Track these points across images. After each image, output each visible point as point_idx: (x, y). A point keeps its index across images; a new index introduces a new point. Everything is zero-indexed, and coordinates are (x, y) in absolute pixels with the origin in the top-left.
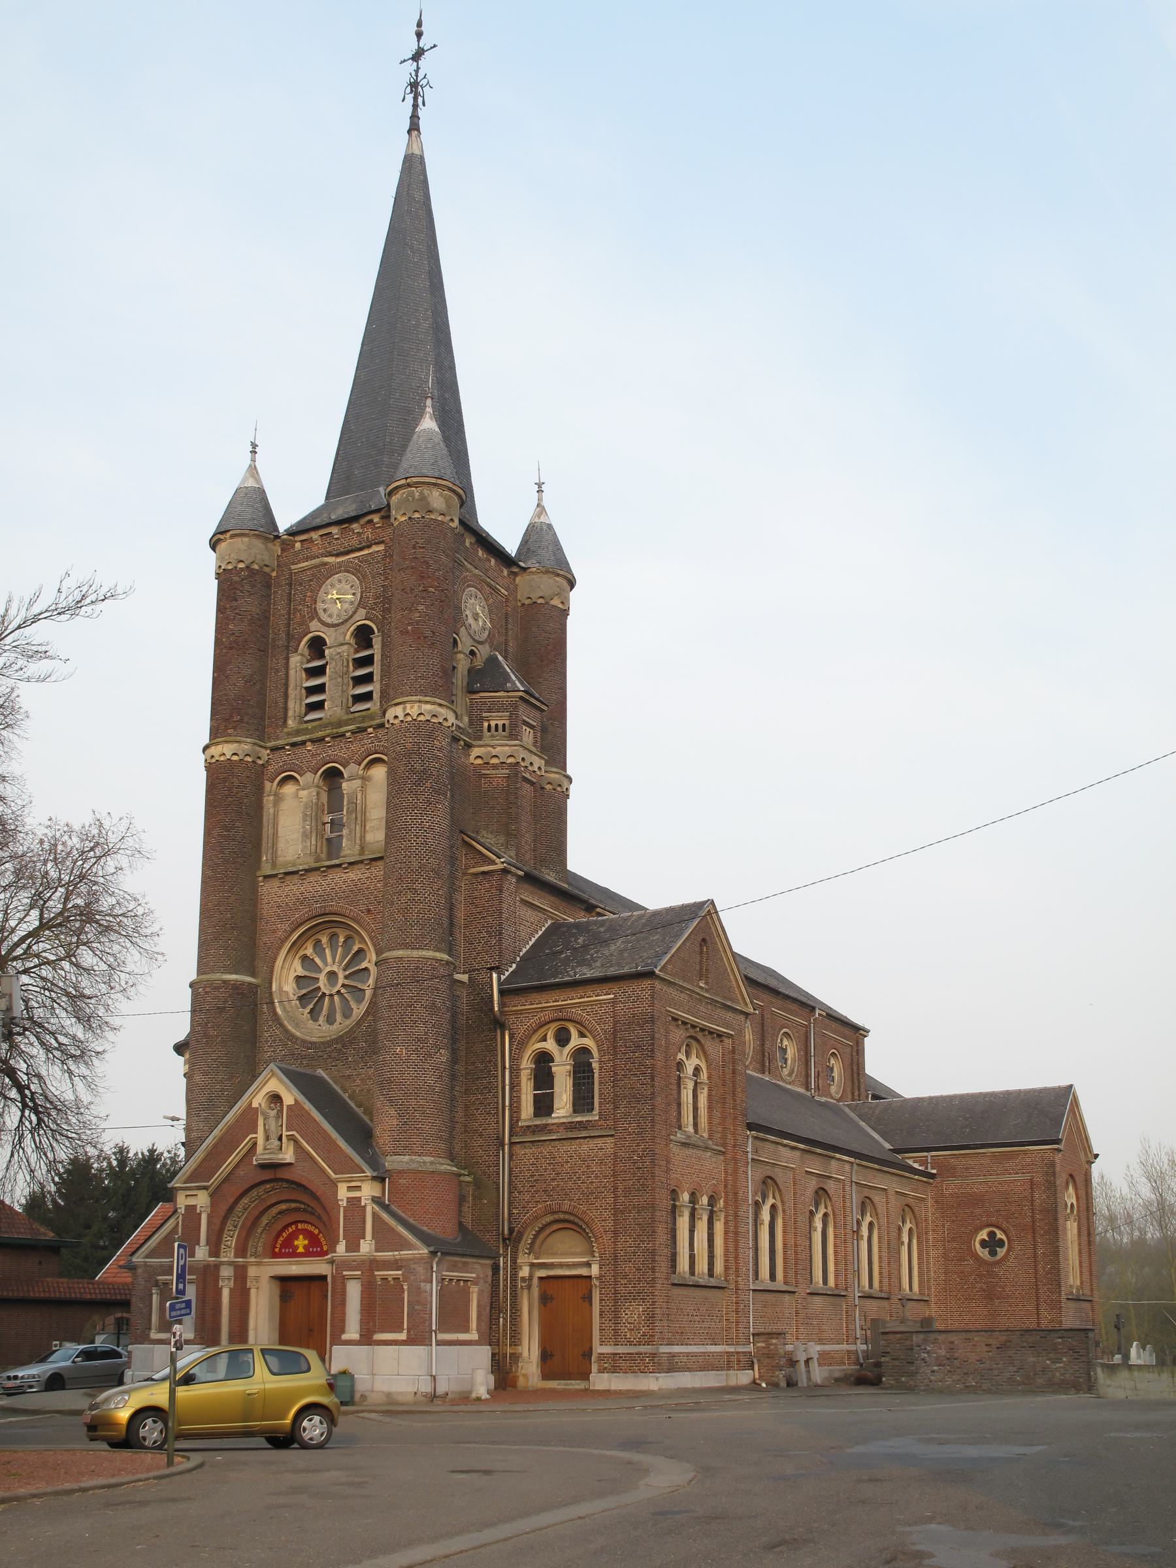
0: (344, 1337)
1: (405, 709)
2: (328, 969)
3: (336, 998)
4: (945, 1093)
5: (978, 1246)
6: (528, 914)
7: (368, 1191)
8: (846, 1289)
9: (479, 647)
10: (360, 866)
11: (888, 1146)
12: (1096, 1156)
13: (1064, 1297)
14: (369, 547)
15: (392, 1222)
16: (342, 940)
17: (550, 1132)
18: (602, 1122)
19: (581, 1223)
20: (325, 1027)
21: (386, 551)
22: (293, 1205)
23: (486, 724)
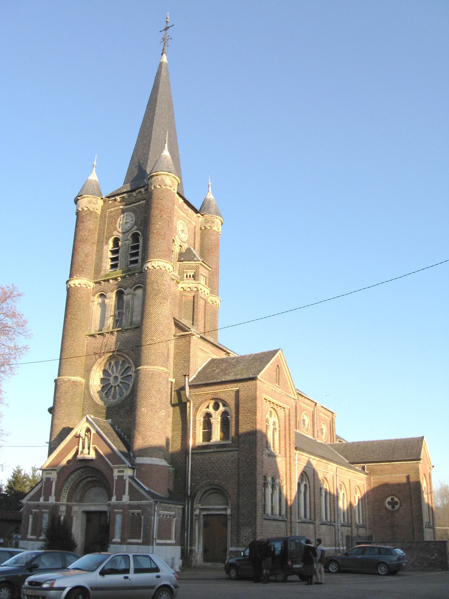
0: (114, 540)
1: (151, 264)
2: (114, 375)
3: (117, 388)
4: (370, 440)
5: (387, 504)
6: (200, 353)
7: (129, 472)
8: (335, 522)
9: (184, 244)
10: (130, 331)
11: (347, 461)
12: (433, 467)
13: (424, 526)
14: (139, 201)
15: (137, 487)
16: (121, 363)
17: (210, 448)
18: (233, 444)
19: (223, 490)
20: (112, 400)
21: (146, 203)
22: (94, 479)
23: (185, 275)
